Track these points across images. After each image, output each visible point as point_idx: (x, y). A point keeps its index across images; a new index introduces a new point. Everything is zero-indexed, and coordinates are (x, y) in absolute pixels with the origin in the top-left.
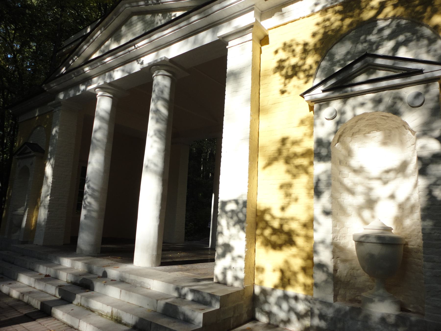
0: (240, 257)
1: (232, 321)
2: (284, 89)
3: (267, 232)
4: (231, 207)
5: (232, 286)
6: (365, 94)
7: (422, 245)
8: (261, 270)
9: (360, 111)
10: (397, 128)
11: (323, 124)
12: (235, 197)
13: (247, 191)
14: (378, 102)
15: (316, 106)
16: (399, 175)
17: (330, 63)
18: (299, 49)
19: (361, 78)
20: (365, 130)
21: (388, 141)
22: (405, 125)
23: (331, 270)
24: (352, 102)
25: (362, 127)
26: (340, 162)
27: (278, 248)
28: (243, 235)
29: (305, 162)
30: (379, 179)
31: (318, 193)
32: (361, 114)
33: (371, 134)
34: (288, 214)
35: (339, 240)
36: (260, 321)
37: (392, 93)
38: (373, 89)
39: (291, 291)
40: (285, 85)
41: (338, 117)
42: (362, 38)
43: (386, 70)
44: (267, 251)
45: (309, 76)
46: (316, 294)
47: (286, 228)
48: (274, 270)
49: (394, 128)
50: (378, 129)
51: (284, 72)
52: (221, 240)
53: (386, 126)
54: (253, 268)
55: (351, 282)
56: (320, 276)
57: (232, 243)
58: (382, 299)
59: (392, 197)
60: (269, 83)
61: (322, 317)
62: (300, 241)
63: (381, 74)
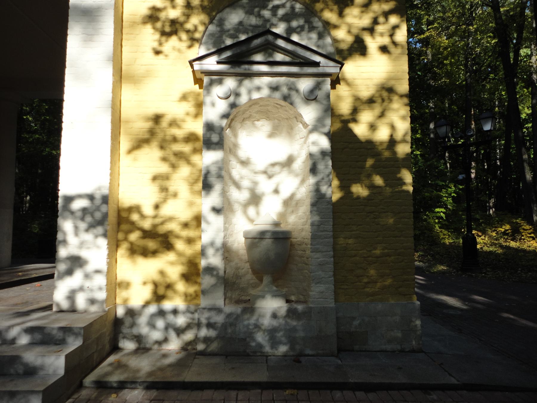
0: (98, 272)
1: (95, 357)
2: (159, 48)
3: (134, 236)
4: (78, 205)
5: (85, 311)
6: (263, 76)
7: (309, 237)
8: (126, 285)
9: (256, 96)
10: (287, 119)
11: (213, 105)
12: (88, 190)
13: (109, 181)
14: (275, 88)
15: (206, 80)
16: (285, 169)
17: (218, 29)
19: (258, 57)
20: (256, 116)
21: (276, 132)
22: (298, 117)
23: (221, 273)
24: (247, 83)
25: (254, 113)
26: (230, 150)
27: (151, 255)
28: (103, 243)
29: (186, 148)
30: (265, 172)
31: (207, 187)
32: (258, 98)
33: (260, 122)
35: (228, 238)
36: (125, 348)
37: (290, 81)
38: (312, 73)
39: (168, 305)
40: (161, 44)
41: (232, 99)
42: (256, 10)
43: (285, 55)
44: (134, 262)
45: (193, 40)
46: (204, 302)
47: (163, 229)
48: (145, 283)
49: (284, 118)
50: (268, 118)
51: (159, 25)
53: (277, 115)
54: (115, 283)
55: (236, 282)
56: (207, 281)
57: (84, 254)
58: (275, 295)
59: (276, 191)
60: (137, 35)
61: (210, 325)
62: (180, 245)
63: (279, 57)
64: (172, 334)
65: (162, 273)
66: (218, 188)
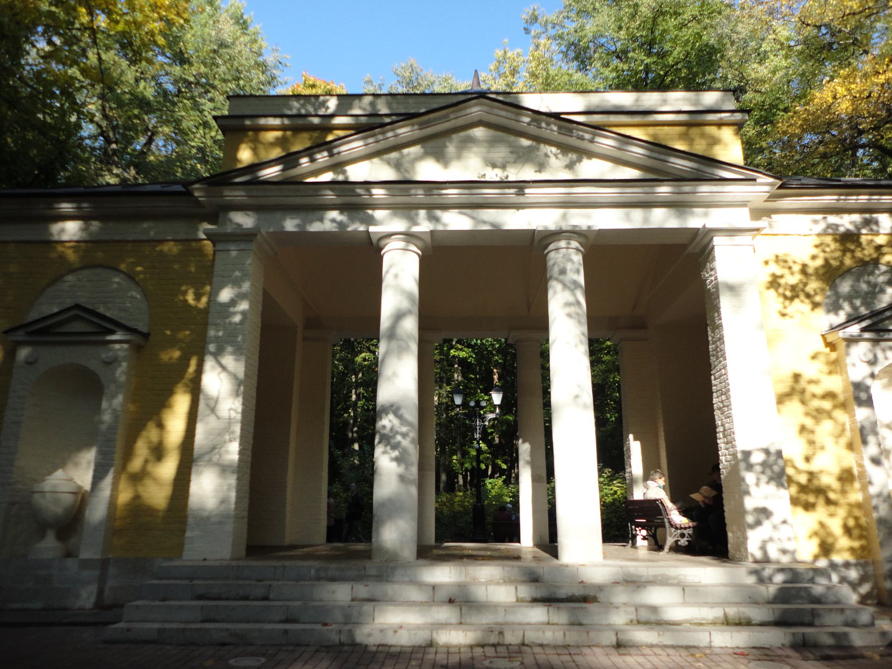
2: (785, 311)
18: (797, 268)
29: (827, 405)
34: (814, 466)
39: (838, 558)
51: (781, 290)
52: (750, 503)
64: (808, 395)
65: (822, 525)
66: (871, 439)
